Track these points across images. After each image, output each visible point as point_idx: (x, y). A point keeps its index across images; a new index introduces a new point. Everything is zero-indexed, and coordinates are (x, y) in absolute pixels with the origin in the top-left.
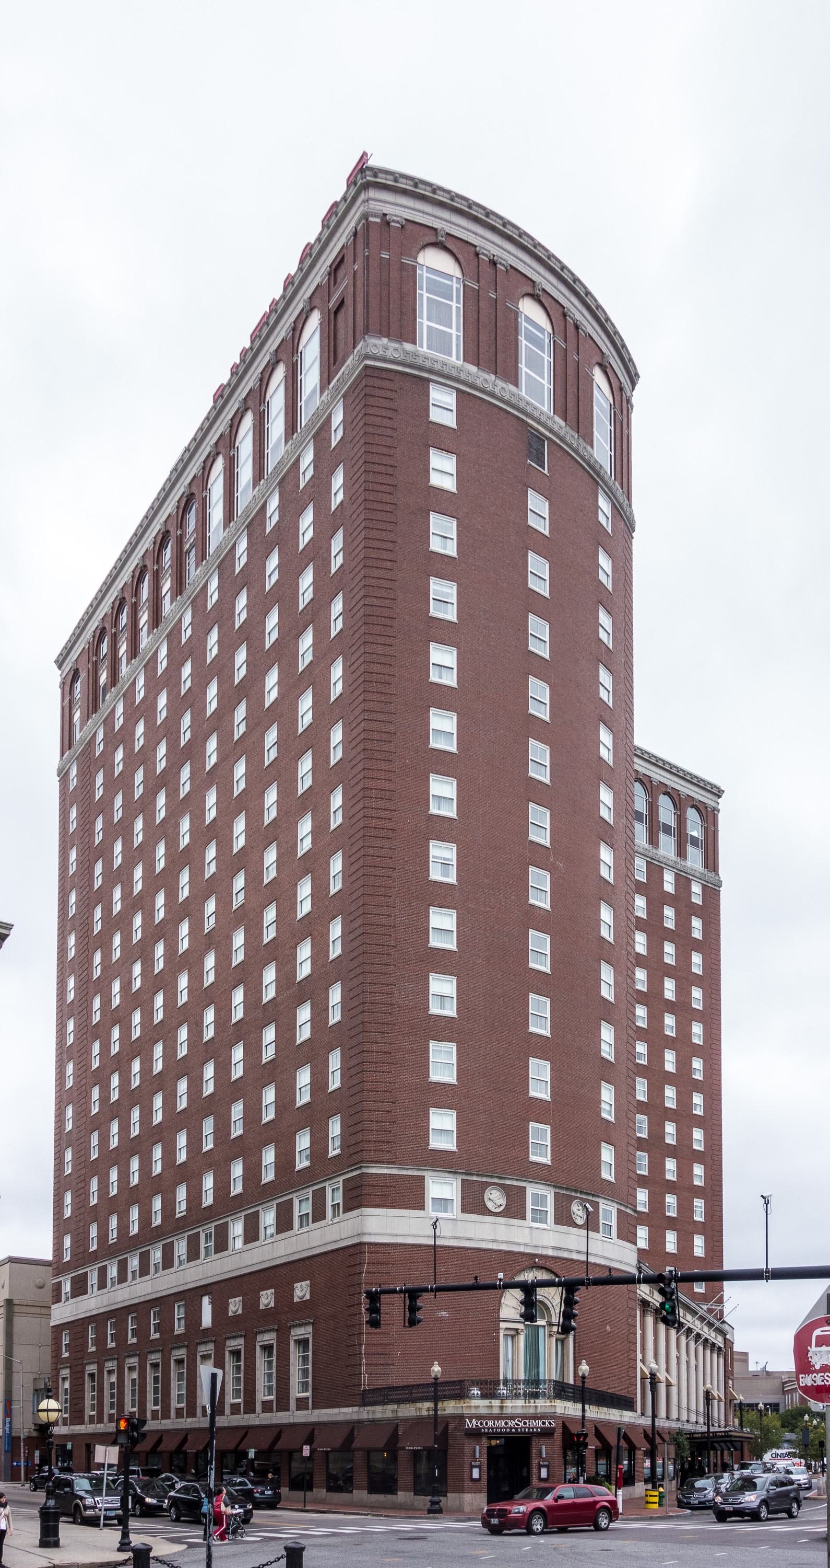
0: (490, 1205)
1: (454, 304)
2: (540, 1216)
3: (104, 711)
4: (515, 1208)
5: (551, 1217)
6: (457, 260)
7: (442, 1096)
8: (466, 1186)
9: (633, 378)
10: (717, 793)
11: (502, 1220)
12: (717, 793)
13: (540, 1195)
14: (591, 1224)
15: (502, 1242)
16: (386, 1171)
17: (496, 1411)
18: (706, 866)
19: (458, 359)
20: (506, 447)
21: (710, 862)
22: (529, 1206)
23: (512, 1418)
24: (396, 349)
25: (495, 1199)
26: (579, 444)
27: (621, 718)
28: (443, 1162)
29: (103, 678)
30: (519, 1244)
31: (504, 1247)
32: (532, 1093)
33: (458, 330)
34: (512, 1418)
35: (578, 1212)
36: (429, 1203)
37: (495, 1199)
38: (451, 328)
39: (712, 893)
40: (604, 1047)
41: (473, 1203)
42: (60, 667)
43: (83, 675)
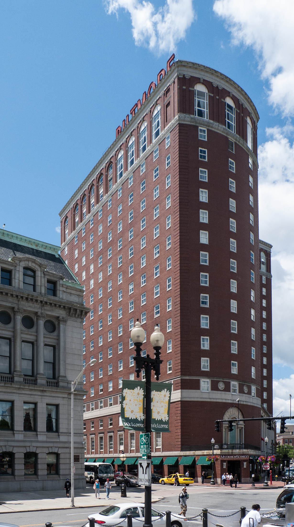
0: (220, 388)
1: (206, 101)
2: (235, 391)
3: (77, 228)
4: (227, 389)
5: (237, 391)
6: (205, 85)
7: (205, 353)
8: (212, 382)
9: (258, 119)
10: (271, 246)
11: (223, 392)
12: (271, 246)
13: (234, 384)
14: (249, 393)
15: (192, 398)
16: (188, 378)
17: (231, 453)
18: (267, 271)
19: (207, 118)
20: (218, 142)
21: (268, 269)
22: (232, 388)
23: (236, 455)
24: (188, 117)
25: (221, 386)
26: (244, 143)
27: (255, 229)
28: (205, 374)
29: (77, 219)
30: (228, 400)
31: (224, 401)
32: (232, 352)
33: (207, 109)
34: (236, 455)
35: (246, 389)
36: (231, 390)
37: (221, 386)
38: (204, 109)
39: (269, 281)
40: (252, 336)
41: (215, 387)
42: (60, 216)
43: (69, 218)
